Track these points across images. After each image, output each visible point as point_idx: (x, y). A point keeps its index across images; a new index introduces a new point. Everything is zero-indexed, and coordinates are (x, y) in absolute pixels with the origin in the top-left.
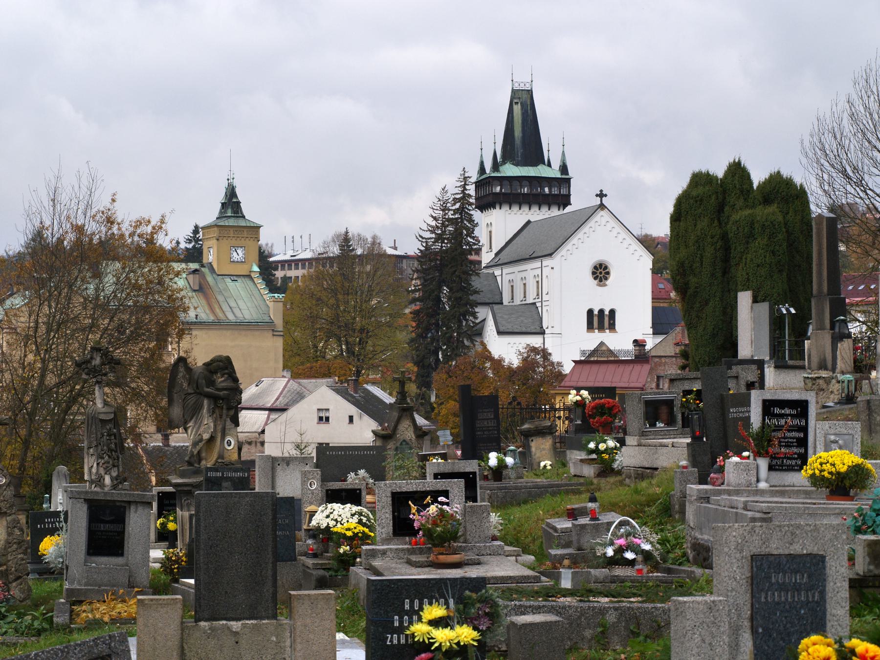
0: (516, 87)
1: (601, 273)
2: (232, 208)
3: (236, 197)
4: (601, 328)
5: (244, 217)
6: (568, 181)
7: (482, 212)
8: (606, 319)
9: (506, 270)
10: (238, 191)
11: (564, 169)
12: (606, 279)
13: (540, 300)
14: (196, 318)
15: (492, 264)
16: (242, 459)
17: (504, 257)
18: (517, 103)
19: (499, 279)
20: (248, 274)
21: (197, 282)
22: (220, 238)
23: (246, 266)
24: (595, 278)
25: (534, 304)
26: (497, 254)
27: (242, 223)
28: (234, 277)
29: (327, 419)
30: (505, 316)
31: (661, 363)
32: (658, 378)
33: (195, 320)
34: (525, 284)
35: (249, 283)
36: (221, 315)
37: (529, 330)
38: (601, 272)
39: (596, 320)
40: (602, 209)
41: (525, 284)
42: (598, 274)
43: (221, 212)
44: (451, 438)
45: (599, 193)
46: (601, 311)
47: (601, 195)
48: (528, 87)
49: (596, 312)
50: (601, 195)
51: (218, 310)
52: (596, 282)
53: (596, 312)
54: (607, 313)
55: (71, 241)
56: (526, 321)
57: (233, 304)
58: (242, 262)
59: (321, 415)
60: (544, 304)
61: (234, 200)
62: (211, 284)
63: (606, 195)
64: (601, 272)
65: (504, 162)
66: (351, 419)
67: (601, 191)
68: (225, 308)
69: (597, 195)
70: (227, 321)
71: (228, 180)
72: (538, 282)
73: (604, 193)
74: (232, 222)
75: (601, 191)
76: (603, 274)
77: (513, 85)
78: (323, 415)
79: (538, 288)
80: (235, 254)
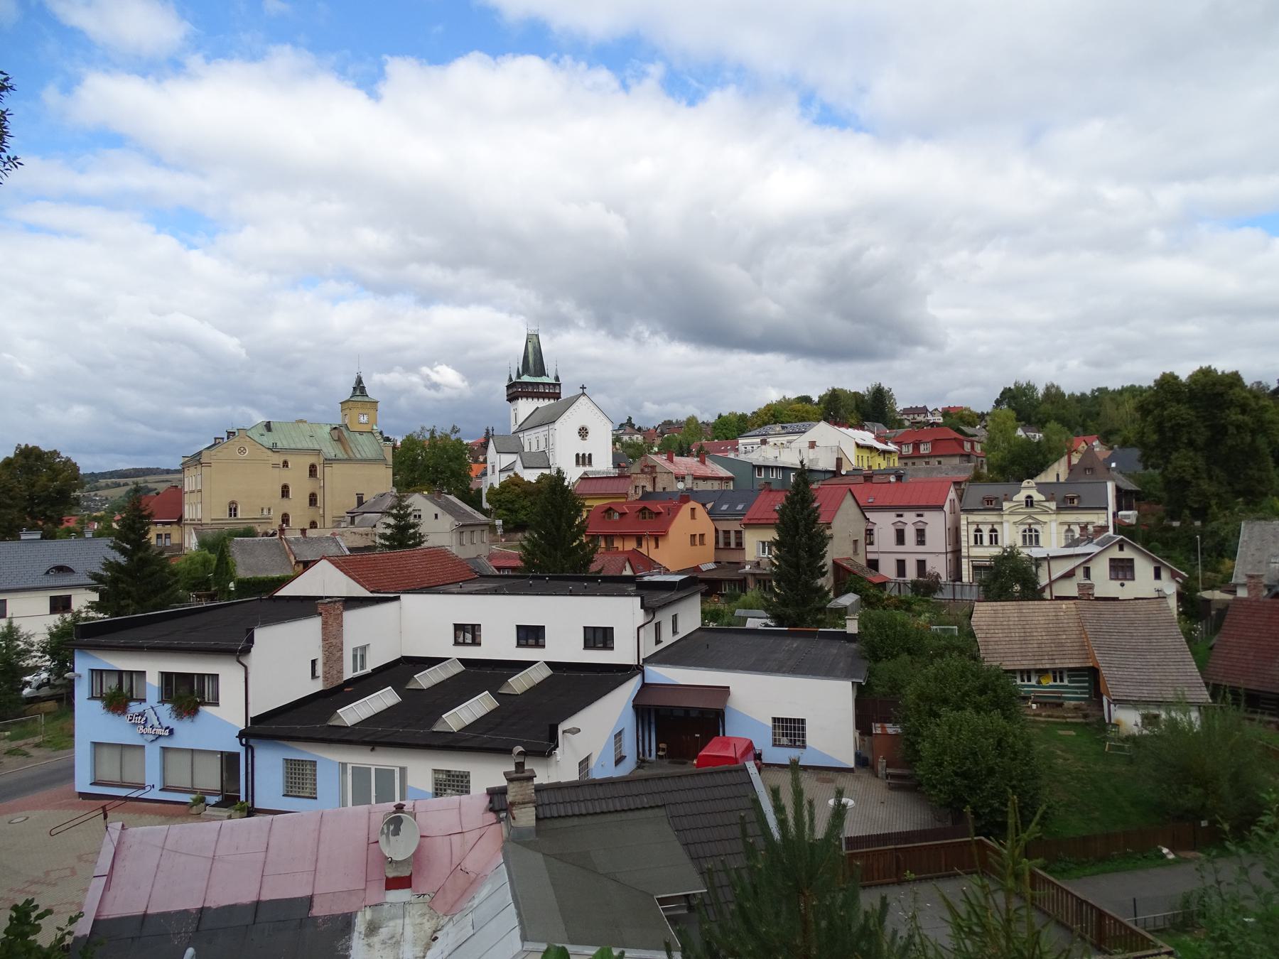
0: (530, 332)
4: (584, 464)
6: (559, 385)
8: (587, 459)
9: (526, 433)
10: (363, 380)
11: (557, 378)
16: (1112, 722)
19: (522, 439)
23: (370, 426)
28: (361, 433)
29: (420, 516)
32: (636, 487)
36: (351, 454)
38: (583, 432)
39: (581, 459)
46: (584, 455)
47: (583, 388)
50: (583, 388)
55: (161, 553)
64: (583, 432)
66: (436, 516)
68: (355, 450)
74: (360, 399)
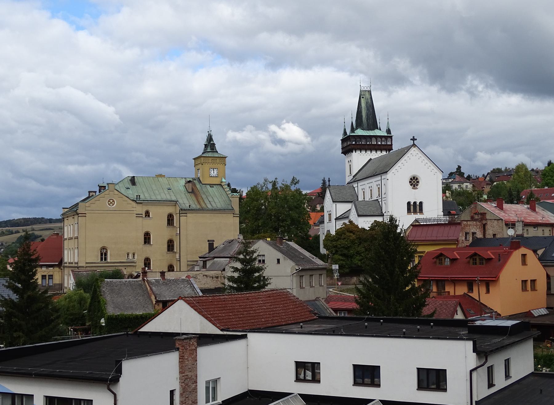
1: (414, 182)
2: (211, 147)
3: (213, 140)
4: (415, 212)
5: (217, 152)
6: (391, 137)
7: (345, 155)
8: (418, 207)
10: (213, 138)
11: (389, 131)
12: (417, 185)
13: (381, 197)
14: (190, 207)
15: (351, 181)
17: (358, 177)
18: (363, 97)
19: (356, 189)
20: (220, 183)
21: (191, 187)
22: (204, 164)
24: (411, 185)
25: (377, 200)
26: (354, 177)
27: (216, 155)
28: (212, 185)
30: (362, 207)
31: (467, 224)
32: (466, 234)
33: (189, 208)
34: (371, 190)
35: (221, 188)
36: (203, 205)
37: (375, 214)
38: (414, 182)
39: (412, 207)
40: (415, 147)
41: (371, 190)
42: (413, 181)
43: (205, 150)
44: (165, 274)
45: (412, 138)
46: (415, 203)
47: (414, 139)
48: (368, 89)
49: (412, 203)
51: (202, 203)
52: (411, 187)
53: (412, 203)
54: (418, 204)
56: (373, 209)
57: (211, 199)
58: (216, 177)
59: (259, 259)
60: (383, 199)
61: (212, 142)
62: (199, 189)
63: (416, 139)
64: (414, 182)
65: (357, 129)
66: (278, 261)
67: (414, 137)
69: (411, 139)
70: (207, 208)
71: (208, 132)
72: (379, 188)
73: (415, 138)
74: (210, 155)
75: (414, 137)
76: (415, 182)
77: (361, 88)
78: (261, 259)
79: (379, 191)
80: (212, 172)
